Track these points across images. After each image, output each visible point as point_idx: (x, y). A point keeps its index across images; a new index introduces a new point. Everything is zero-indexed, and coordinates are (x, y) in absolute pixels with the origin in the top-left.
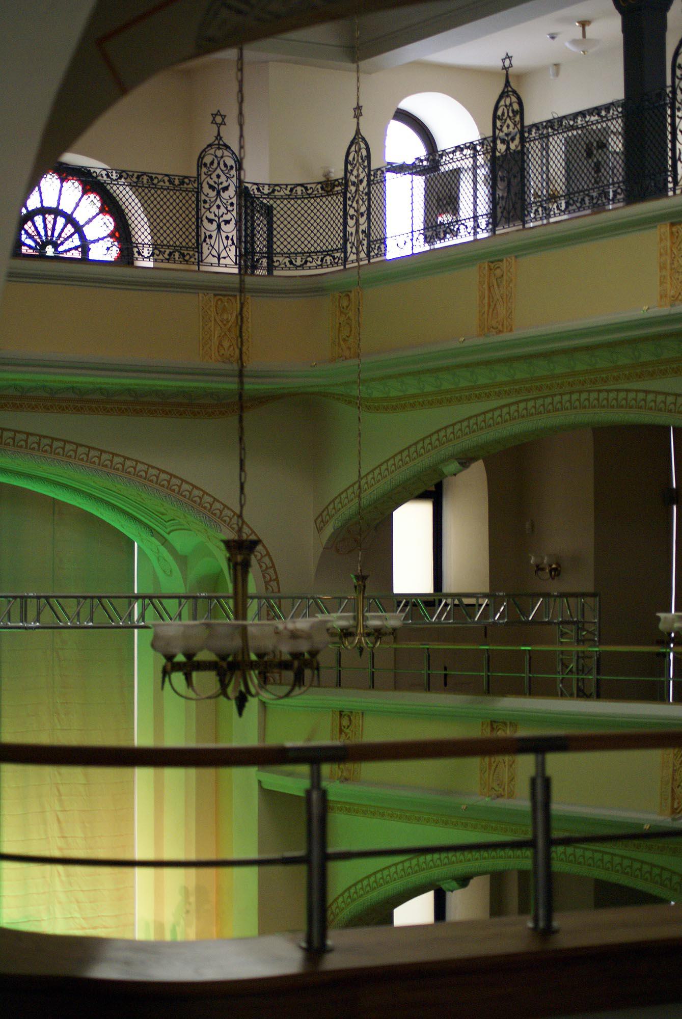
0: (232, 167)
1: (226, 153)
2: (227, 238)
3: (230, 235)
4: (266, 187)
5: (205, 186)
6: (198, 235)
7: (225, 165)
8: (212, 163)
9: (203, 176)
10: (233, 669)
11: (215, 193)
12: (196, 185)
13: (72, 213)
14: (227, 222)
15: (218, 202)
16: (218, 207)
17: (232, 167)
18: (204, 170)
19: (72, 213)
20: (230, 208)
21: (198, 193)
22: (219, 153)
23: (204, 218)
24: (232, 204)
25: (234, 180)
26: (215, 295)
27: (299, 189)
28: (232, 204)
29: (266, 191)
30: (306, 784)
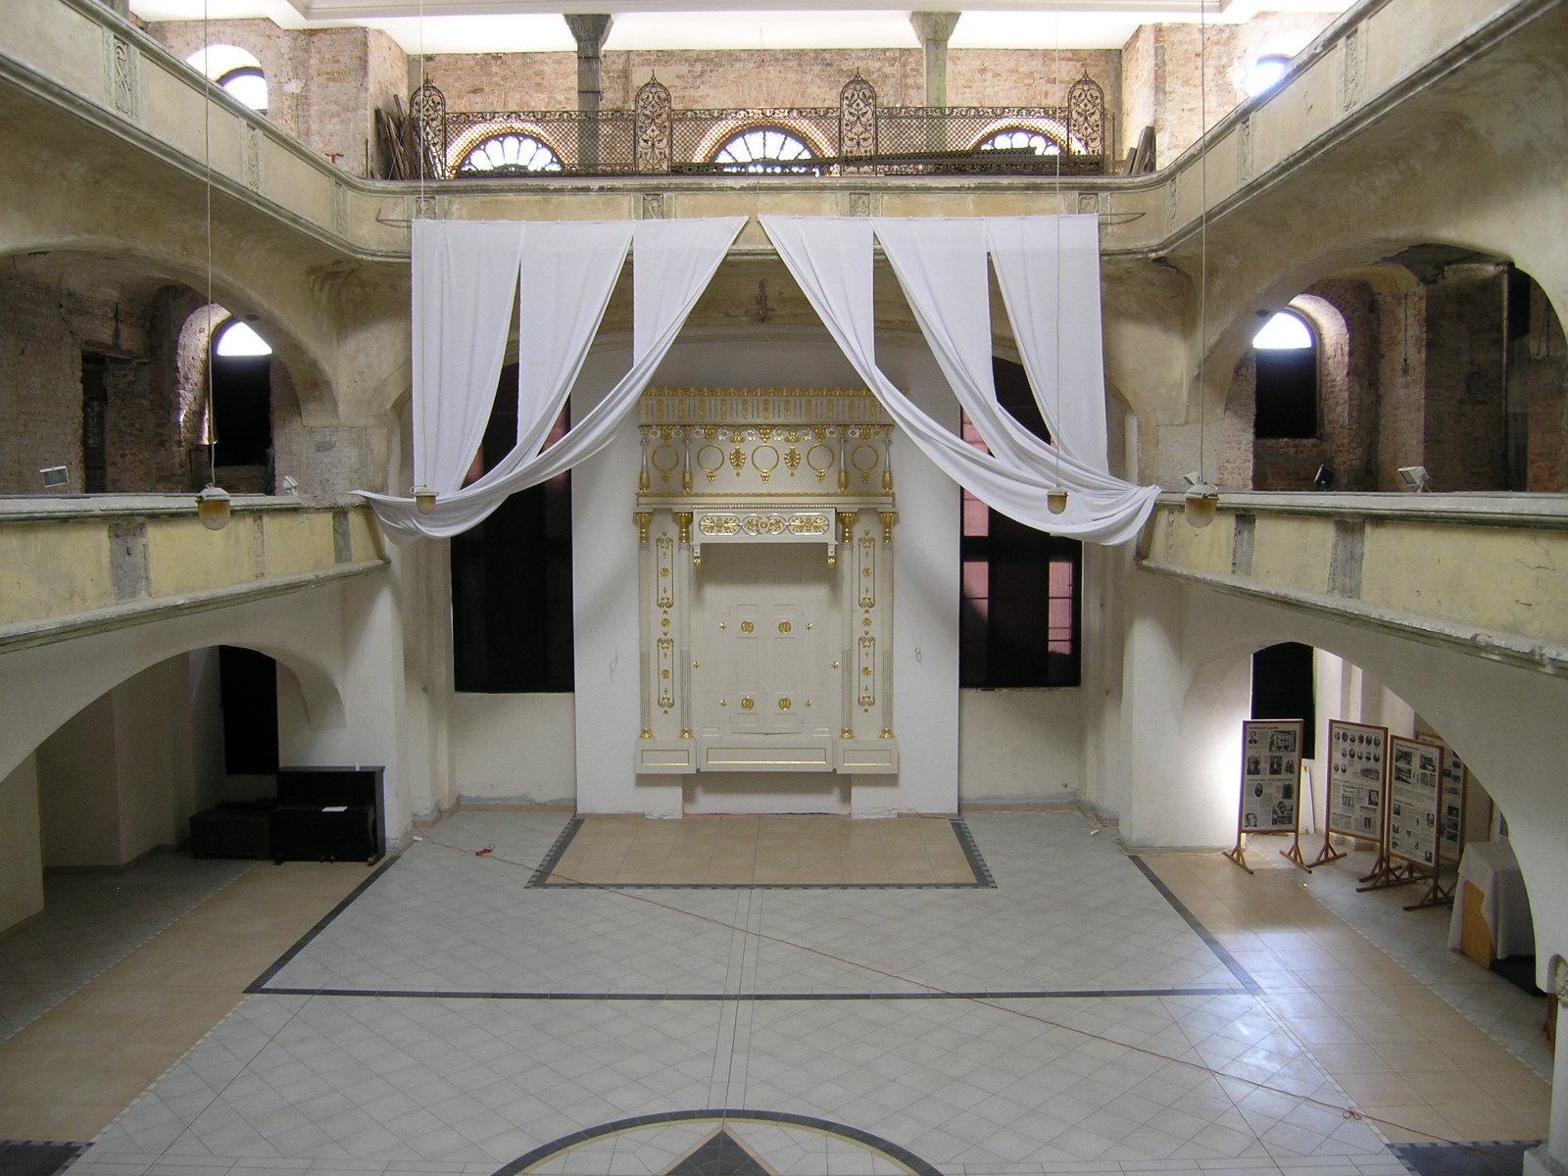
0: (1097, 97)
1: (1092, 87)
2: (660, 153)
3: (868, 149)
4: (716, 112)
5: (846, 113)
6: (635, 153)
7: (433, 102)
8: (853, 95)
9: (845, 107)
10: (1345, 575)
11: (1083, 118)
12: (1066, 113)
13: (785, 138)
14: (1093, 140)
15: (1086, 125)
16: (1086, 128)
17: (1097, 97)
18: (846, 102)
19: (785, 138)
20: (869, 128)
21: (840, 120)
22: (653, 90)
23: (640, 140)
24: (1097, 126)
25: (1099, 107)
26: (1080, 194)
27: (973, 111)
28: (1097, 126)
29: (716, 114)
30: (1292, 843)
